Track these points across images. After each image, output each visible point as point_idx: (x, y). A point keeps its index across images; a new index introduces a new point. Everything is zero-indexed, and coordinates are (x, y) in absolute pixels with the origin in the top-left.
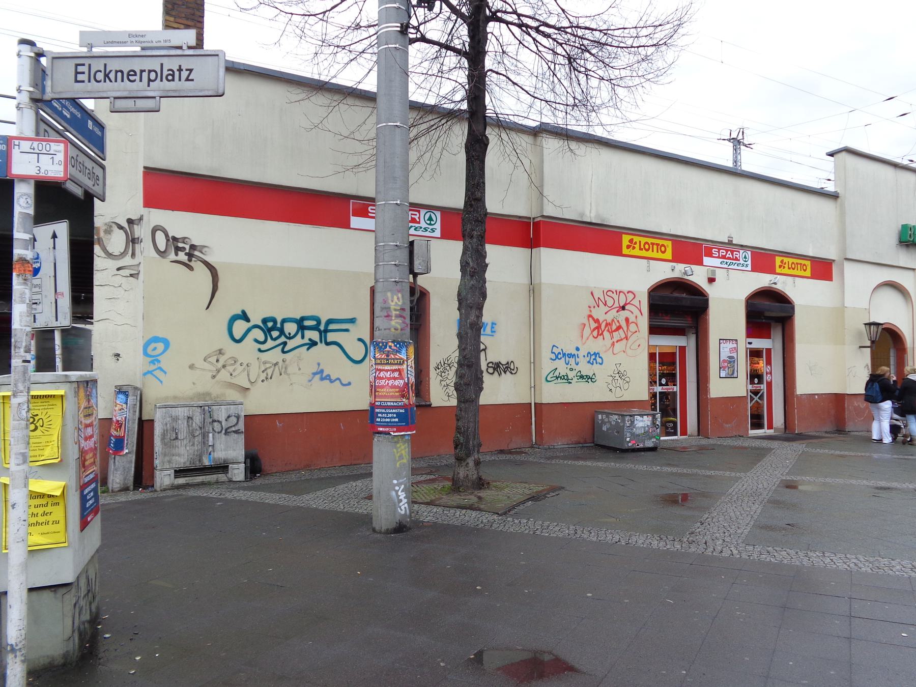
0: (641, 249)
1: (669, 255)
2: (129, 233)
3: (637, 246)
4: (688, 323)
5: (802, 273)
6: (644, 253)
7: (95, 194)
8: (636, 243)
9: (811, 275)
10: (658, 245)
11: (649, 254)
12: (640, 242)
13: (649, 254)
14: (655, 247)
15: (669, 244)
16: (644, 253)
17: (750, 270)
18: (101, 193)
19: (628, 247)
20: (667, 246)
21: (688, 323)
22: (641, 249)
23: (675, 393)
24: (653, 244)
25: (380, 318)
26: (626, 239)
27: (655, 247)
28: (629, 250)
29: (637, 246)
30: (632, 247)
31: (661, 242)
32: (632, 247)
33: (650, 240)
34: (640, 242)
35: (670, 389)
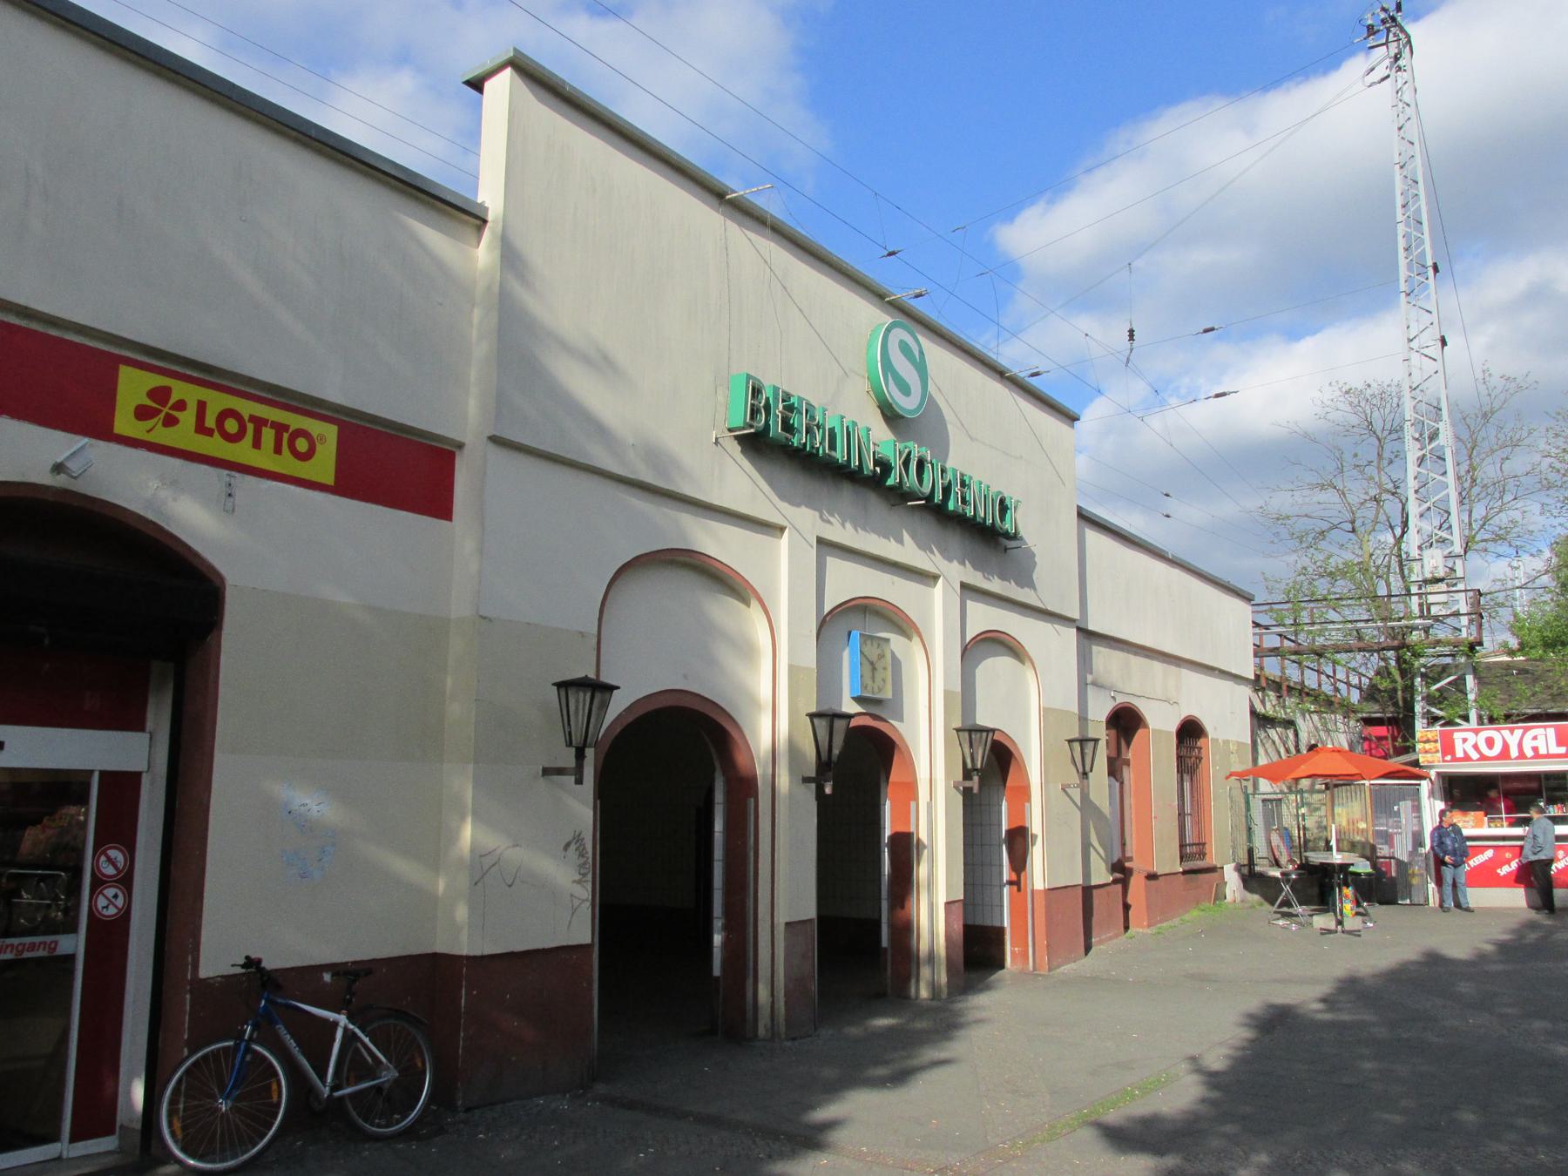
0: (201, 428)
1: (324, 466)
2: (228, 1089)
3: (188, 418)
4: (1299, 838)
5: (286, 463)
6: (215, 446)
7: (754, 591)
8: (181, 405)
9: (337, 478)
10: (280, 428)
11: (242, 452)
12: (202, 406)
13: (242, 452)
14: (268, 435)
15: (327, 434)
16: (215, 446)
17: (329, 479)
18: (969, 603)
19: (142, 413)
20: (322, 438)
21: (1299, 838)
22: (201, 428)
23: (70, 958)
24: (259, 423)
25: (476, 1111)
26: (133, 387)
27: (268, 435)
28: (150, 423)
29: (188, 418)
30: (162, 416)
31: (295, 421)
32: (162, 416)
33: (247, 408)
34: (202, 406)
35: (33, 947)
